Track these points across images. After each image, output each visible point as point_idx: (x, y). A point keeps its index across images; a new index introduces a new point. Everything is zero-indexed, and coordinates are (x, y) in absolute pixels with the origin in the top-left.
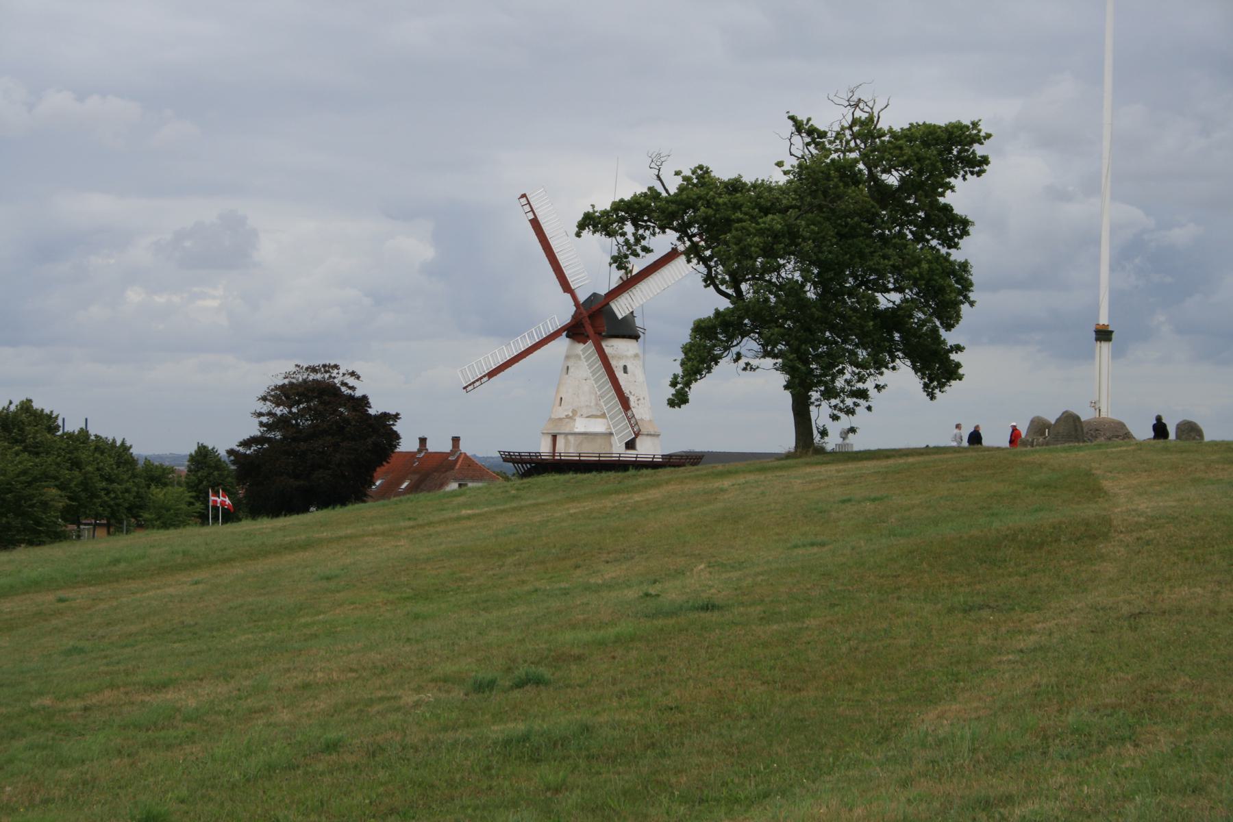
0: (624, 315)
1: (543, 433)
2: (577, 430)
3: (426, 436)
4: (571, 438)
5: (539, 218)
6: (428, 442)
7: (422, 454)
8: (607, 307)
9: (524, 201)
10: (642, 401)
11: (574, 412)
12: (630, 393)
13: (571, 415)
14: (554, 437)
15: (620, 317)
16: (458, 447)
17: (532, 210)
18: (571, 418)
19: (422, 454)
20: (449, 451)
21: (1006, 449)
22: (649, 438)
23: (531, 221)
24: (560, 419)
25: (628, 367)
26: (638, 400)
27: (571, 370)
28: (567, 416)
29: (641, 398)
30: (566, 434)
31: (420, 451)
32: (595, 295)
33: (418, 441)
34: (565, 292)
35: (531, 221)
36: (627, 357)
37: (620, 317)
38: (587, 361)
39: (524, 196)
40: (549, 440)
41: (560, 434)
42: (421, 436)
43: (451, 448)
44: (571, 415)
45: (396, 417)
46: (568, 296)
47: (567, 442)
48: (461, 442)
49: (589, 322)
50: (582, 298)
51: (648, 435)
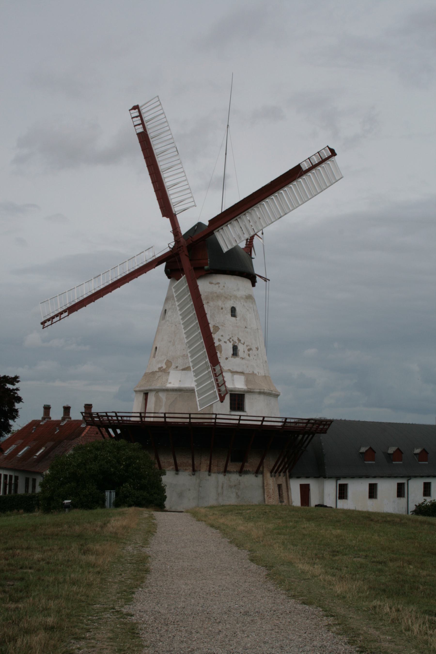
0: (230, 247)
1: (136, 391)
2: (169, 386)
3: (69, 405)
4: (162, 396)
5: (149, 132)
6: (71, 411)
7: (65, 422)
8: (211, 237)
9: (135, 113)
10: (254, 352)
11: (169, 363)
12: (239, 340)
13: (164, 367)
14: (146, 394)
15: (225, 250)
16: (69, 415)
17: (143, 123)
18: (164, 371)
19: (65, 422)
20: (40, 419)
21: (298, 507)
22: (262, 397)
23: (139, 134)
24: (153, 373)
25: (238, 309)
26: (249, 350)
27: (169, 313)
28: (160, 368)
29: (254, 349)
30: (157, 391)
31: (63, 419)
32: (199, 225)
33: (42, 410)
34: (163, 216)
35: (139, 134)
36: (236, 297)
37: (225, 250)
38: (178, 301)
39: (136, 107)
40: (141, 397)
41: (151, 390)
42: (65, 405)
43: (62, 415)
44: (164, 367)
45: (14, 380)
46: (167, 221)
47: (158, 399)
48: (51, 410)
49: (186, 252)
50: (184, 229)
51: (260, 393)
